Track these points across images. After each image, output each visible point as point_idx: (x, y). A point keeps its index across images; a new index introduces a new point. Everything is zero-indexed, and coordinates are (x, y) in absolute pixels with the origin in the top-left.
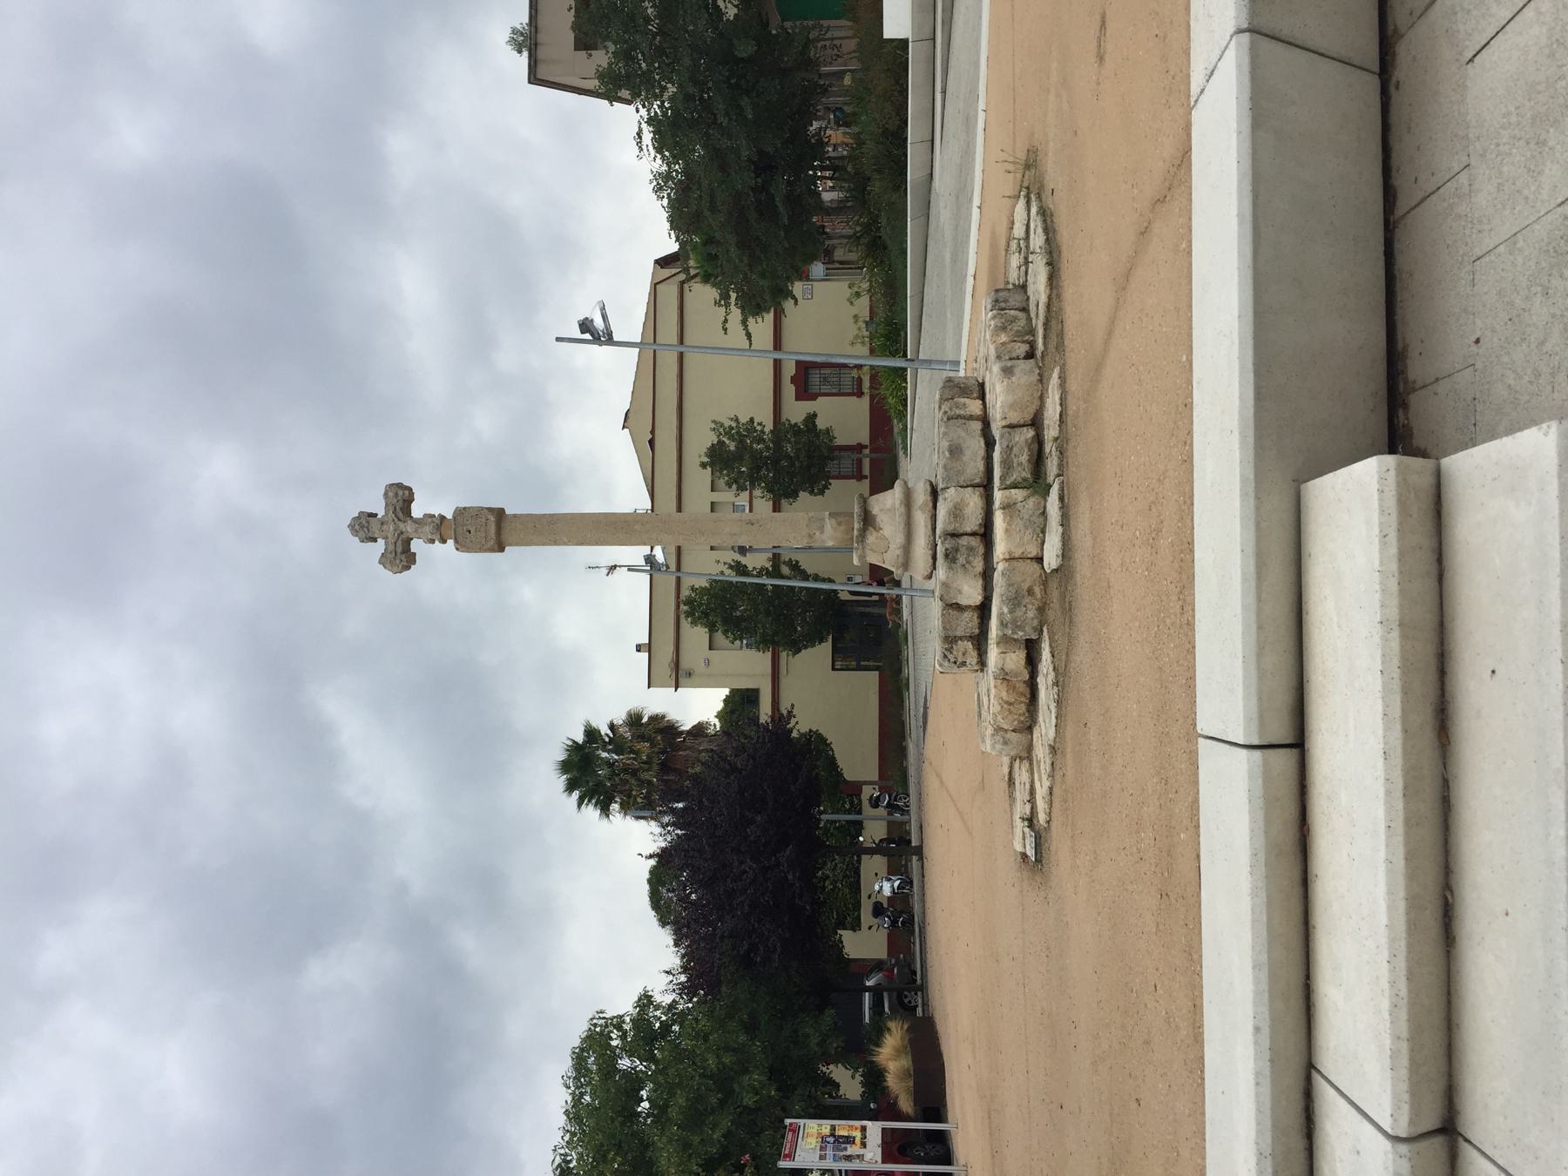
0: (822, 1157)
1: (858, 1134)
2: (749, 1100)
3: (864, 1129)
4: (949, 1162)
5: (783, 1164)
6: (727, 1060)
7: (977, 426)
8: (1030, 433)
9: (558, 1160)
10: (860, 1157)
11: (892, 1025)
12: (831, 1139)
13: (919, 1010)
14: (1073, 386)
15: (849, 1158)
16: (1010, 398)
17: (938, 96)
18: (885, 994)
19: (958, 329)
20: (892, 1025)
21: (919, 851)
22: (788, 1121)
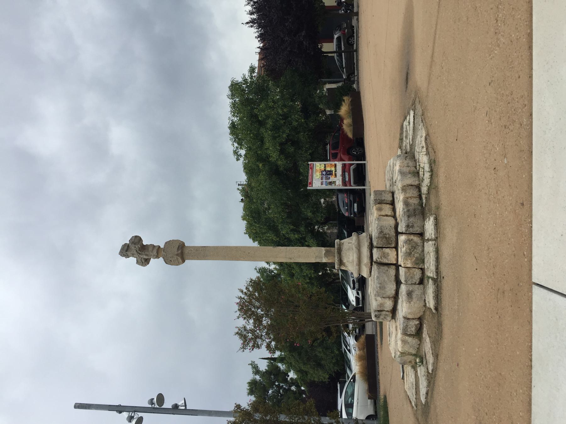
0: (322, 184)
1: (333, 169)
2: (295, 124)
3: (335, 165)
4: (364, 160)
5: (308, 188)
6: (285, 110)
7: (392, 271)
8: (418, 322)
9: (231, 122)
10: (334, 182)
11: (345, 98)
12: (324, 173)
13: (355, 46)
14: (446, 253)
15: (331, 183)
16: (409, 311)
17: (378, 329)
18: (343, 54)
19: (384, 169)
20: (345, 98)
21: (357, 14)
22: (310, 163)
